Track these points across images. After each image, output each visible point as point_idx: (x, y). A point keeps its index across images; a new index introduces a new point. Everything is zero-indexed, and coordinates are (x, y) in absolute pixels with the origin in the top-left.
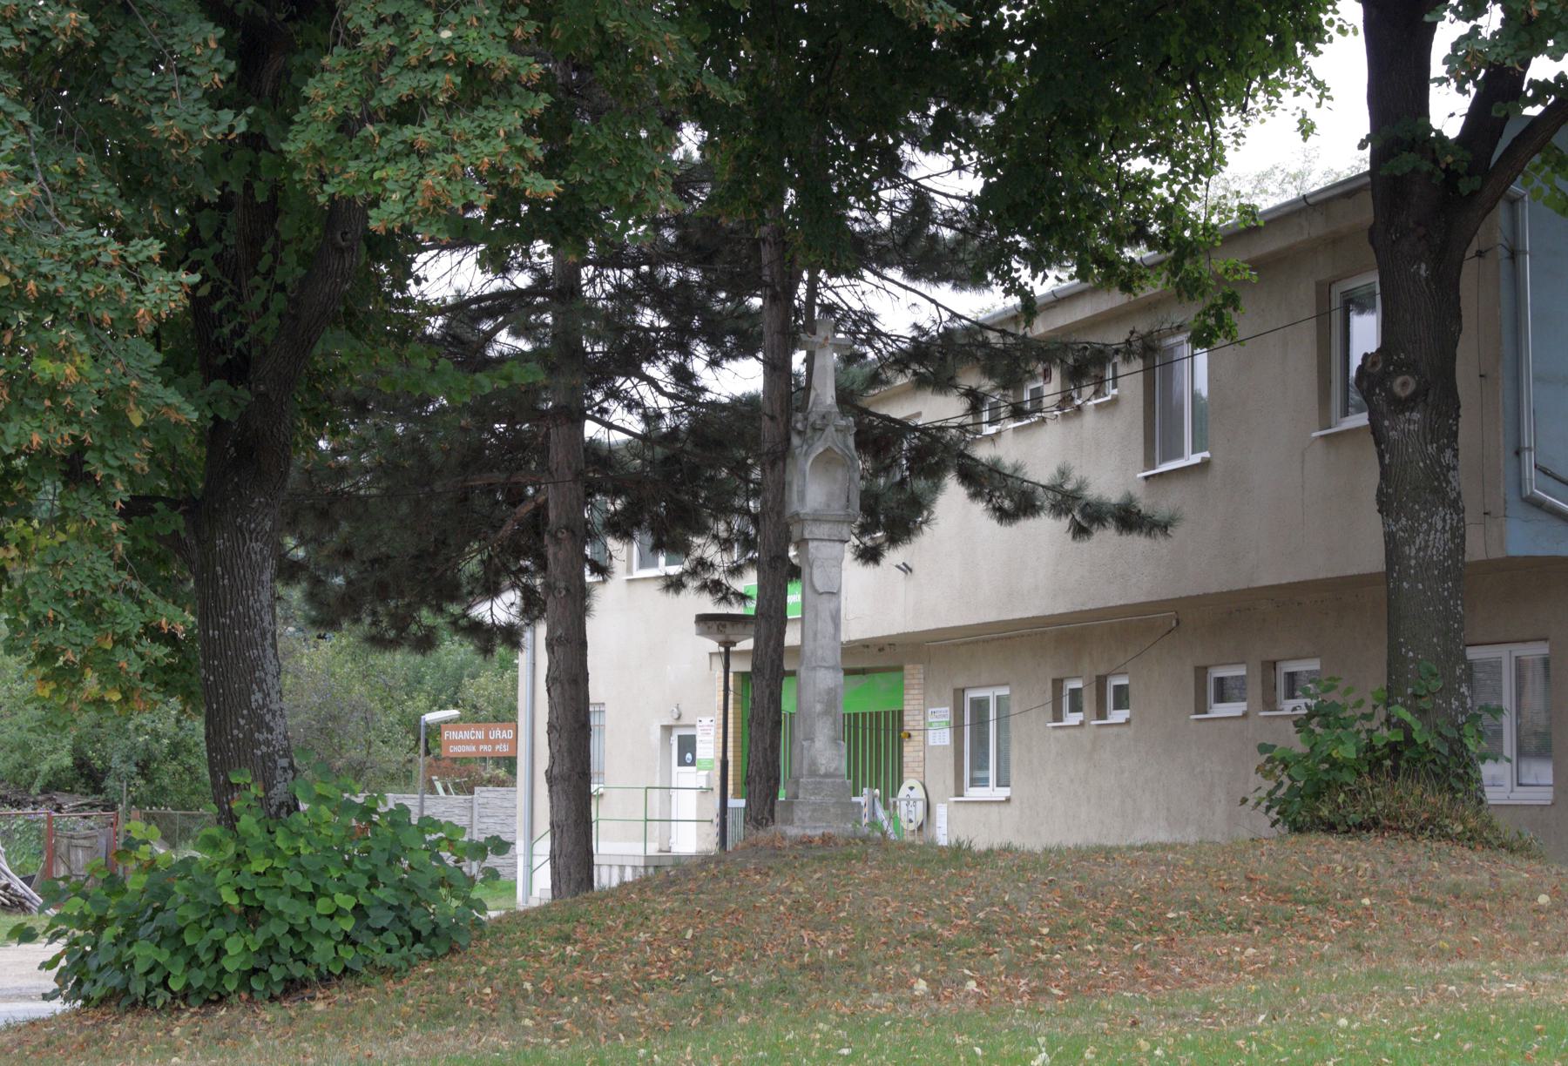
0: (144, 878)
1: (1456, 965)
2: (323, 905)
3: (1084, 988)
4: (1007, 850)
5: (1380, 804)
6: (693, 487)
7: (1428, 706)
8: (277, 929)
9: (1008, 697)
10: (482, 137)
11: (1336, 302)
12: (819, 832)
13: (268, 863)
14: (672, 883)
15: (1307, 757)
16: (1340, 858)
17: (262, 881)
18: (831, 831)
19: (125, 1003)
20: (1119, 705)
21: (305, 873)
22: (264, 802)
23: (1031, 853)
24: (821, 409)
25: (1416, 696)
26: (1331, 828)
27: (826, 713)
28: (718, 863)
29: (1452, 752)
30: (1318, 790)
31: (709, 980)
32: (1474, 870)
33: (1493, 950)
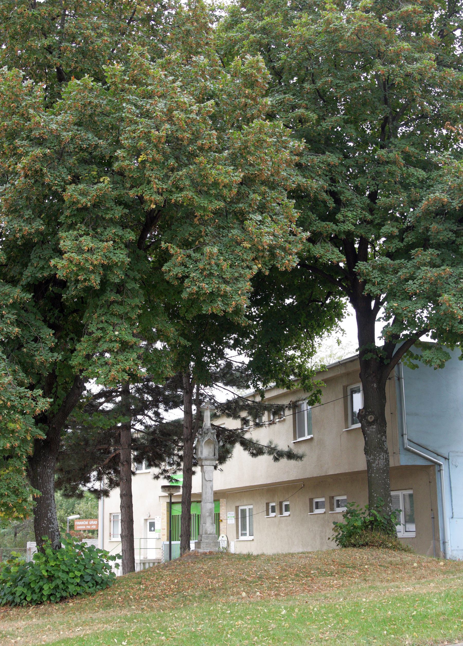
0: (17, 568)
1: (392, 584)
2: (71, 575)
3: (289, 594)
4: (263, 555)
5: (368, 538)
6: (157, 447)
7: (381, 510)
8: (59, 582)
9: (252, 509)
10: (126, 361)
11: (349, 393)
12: (208, 551)
13: (55, 563)
14: (167, 566)
15: (347, 525)
16: (359, 555)
17: (54, 568)
18: (212, 550)
19: (13, 605)
20: (286, 510)
21: (66, 566)
22: (52, 545)
23: (270, 555)
24: (207, 427)
25: (377, 507)
26: (354, 546)
27: (210, 516)
28: (180, 560)
29: (388, 522)
30: (350, 535)
31: (183, 594)
32: (396, 557)
33: (402, 579)
